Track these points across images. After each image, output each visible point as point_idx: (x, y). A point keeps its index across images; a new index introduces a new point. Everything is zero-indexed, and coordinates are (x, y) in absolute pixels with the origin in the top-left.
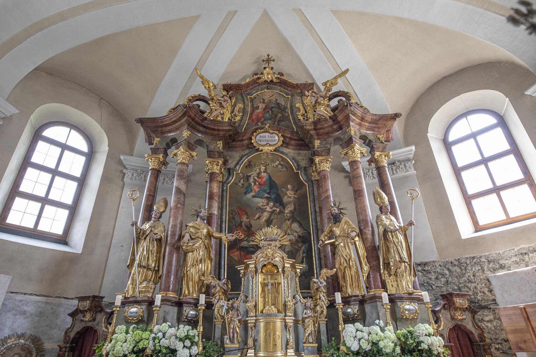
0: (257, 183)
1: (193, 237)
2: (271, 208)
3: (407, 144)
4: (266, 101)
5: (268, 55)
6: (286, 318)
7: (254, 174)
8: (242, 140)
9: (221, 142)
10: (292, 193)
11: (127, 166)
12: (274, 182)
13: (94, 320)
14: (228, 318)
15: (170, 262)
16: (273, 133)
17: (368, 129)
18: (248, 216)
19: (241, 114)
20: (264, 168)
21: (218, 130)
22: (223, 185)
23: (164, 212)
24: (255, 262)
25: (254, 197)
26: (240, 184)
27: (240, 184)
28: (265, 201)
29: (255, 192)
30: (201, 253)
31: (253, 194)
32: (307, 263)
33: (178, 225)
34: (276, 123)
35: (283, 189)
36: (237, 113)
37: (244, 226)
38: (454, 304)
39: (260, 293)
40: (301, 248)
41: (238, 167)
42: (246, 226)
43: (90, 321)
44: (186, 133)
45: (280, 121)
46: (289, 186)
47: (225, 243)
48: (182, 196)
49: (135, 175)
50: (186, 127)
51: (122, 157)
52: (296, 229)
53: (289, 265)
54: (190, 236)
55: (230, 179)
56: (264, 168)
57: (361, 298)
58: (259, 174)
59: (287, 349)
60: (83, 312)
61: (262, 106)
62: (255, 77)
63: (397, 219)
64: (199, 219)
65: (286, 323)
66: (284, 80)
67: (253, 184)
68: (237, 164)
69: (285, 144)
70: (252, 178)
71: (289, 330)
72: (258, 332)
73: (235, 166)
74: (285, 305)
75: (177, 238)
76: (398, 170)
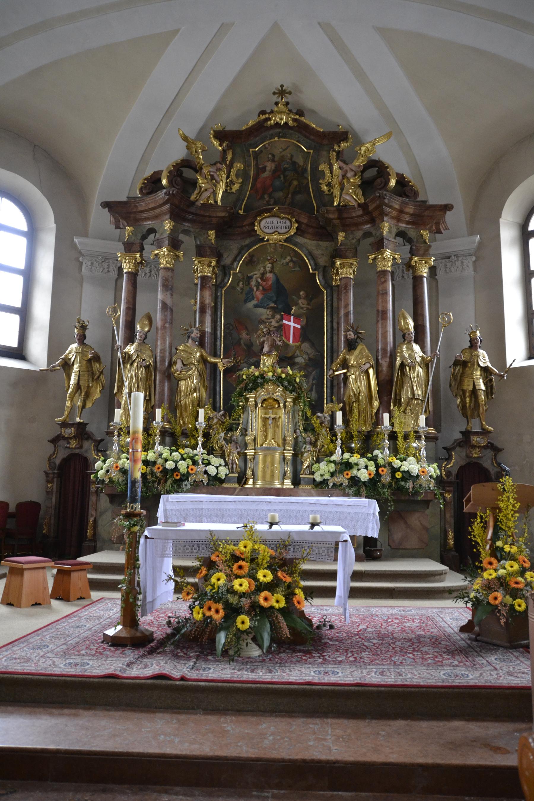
0: (261, 288)
1: (185, 363)
2: (277, 322)
3: (472, 233)
4: (276, 158)
5: (282, 86)
6: (285, 451)
7: (256, 274)
8: (242, 226)
9: (214, 232)
10: (305, 302)
11: (83, 252)
12: (283, 286)
13: (81, 447)
14: (227, 450)
15: (162, 391)
16: (283, 218)
17: (408, 223)
18: (248, 331)
19: (240, 180)
20: (270, 265)
21: (210, 217)
22: (216, 290)
23: (149, 331)
24: (255, 396)
25: (256, 306)
26: (238, 289)
27: (238, 289)
28: (269, 312)
29: (258, 300)
30: (195, 381)
31: (254, 302)
32: (317, 392)
33: (168, 349)
34: (290, 196)
35: (294, 297)
36: (235, 179)
37: (243, 345)
38: (470, 441)
39: (259, 427)
40: (311, 373)
41: (235, 264)
42: (246, 345)
43: (75, 448)
44: (168, 225)
45: (295, 193)
46: (302, 293)
47: (221, 368)
48: (169, 312)
49: (96, 264)
50: (168, 216)
51: (76, 240)
52: (307, 350)
53: (290, 400)
54: (183, 363)
55: (226, 281)
56: (270, 265)
57: (366, 434)
58: (263, 274)
59: (284, 479)
60: (67, 439)
61: (270, 166)
62: (263, 117)
63: (423, 348)
64: (190, 341)
65: (284, 456)
66: (305, 123)
67: (255, 288)
68: (235, 260)
69: (300, 231)
70: (254, 280)
71: (287, 463)
72: (257, 464)
73: (232, 263)
74: (284, 440)
75: (167, 364)
76: (452, 269)
